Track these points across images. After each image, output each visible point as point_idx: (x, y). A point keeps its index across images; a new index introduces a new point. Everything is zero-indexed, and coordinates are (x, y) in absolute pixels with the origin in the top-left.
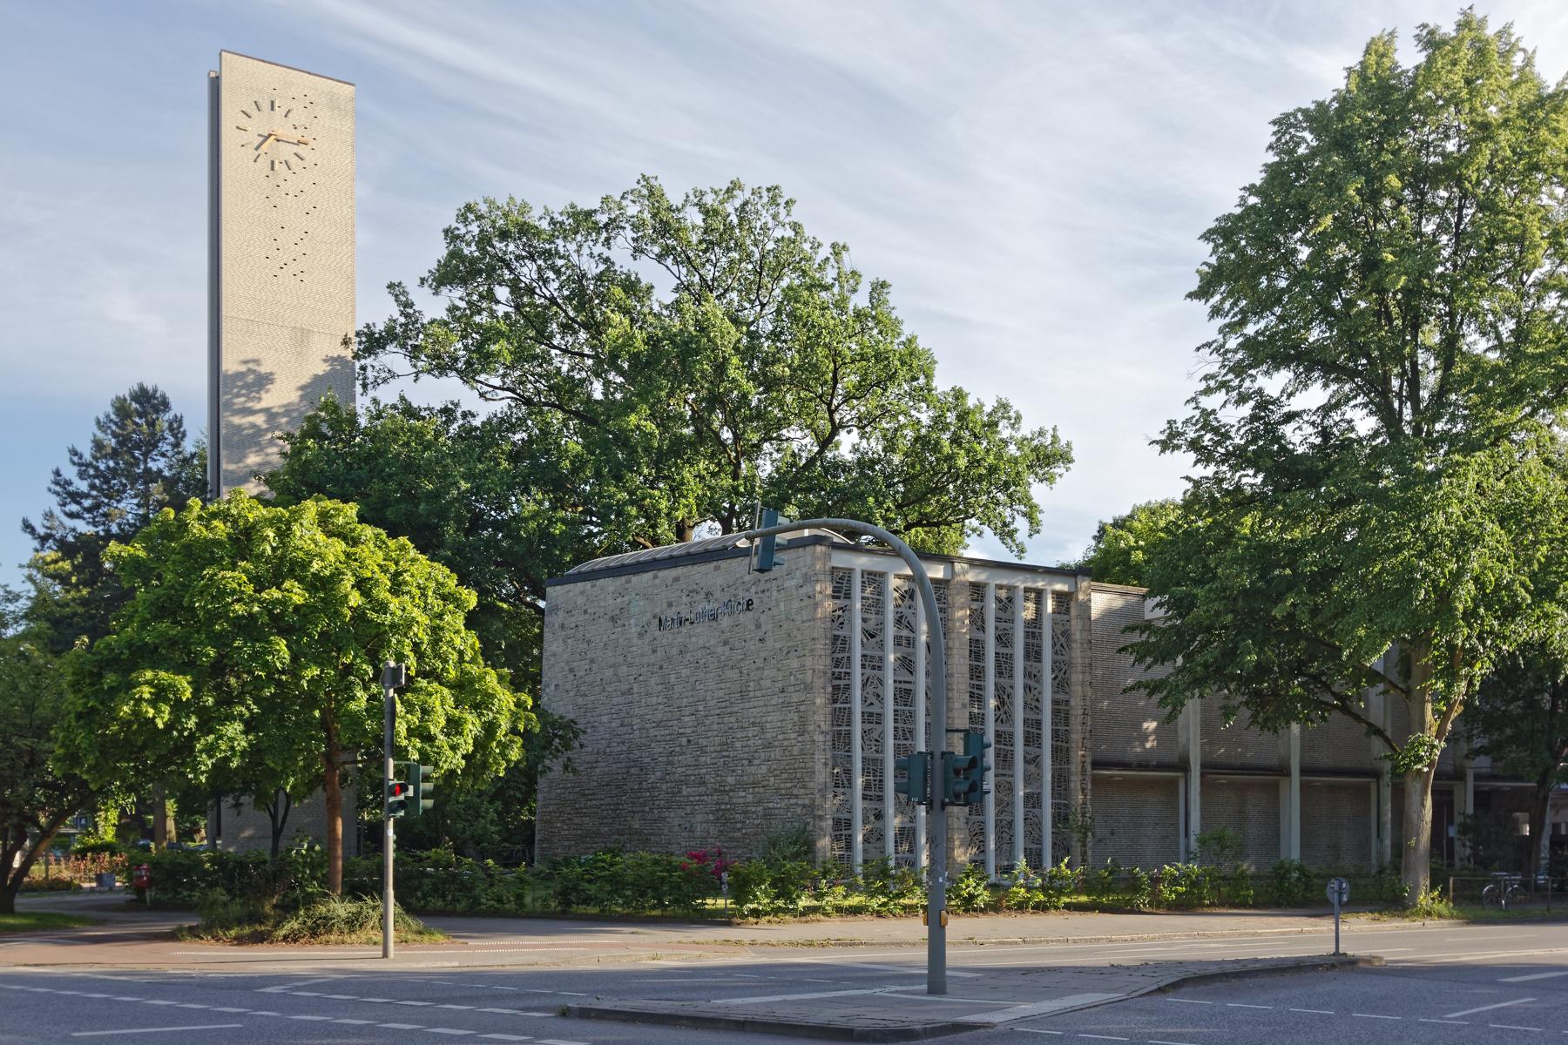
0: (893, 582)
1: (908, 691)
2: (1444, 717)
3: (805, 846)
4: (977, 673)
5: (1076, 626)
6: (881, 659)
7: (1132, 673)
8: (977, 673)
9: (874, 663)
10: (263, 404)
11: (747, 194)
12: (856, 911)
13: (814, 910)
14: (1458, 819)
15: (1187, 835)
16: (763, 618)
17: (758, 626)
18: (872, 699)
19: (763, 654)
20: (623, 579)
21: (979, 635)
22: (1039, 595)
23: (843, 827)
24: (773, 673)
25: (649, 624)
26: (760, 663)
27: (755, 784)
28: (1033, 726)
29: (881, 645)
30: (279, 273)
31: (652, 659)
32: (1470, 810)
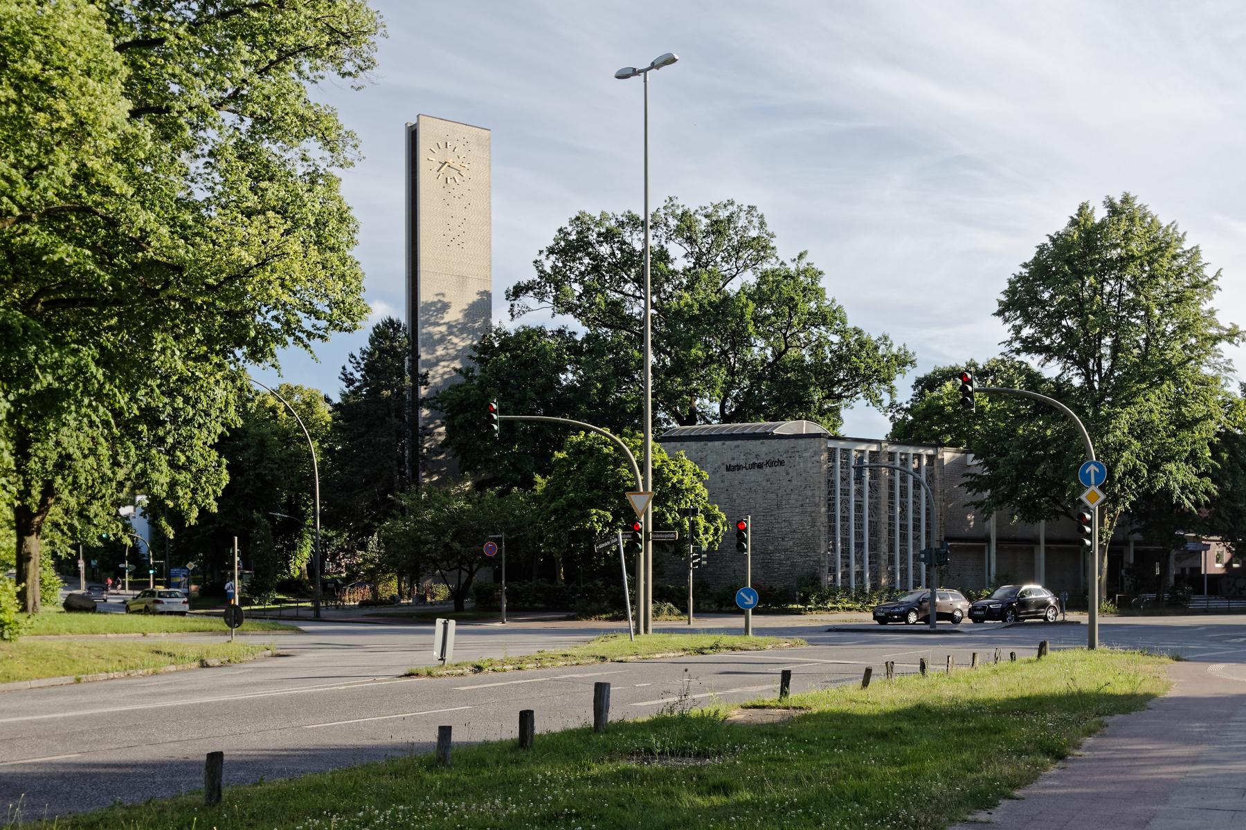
0: (854, 453)
1: (860, 506)
2: (1112, 520)
3: (814, 580)
4: (892, 496)
5: (937, 471)
6: (848, 490)
7: (968, 496)
8: (892, 496)
9: (845, 493)
10: (446, 320)
11: (735, 208)
12: (849, 609)
13: (832, 608)
14: (1126, 566)
15: (989, 574)
16: (790, 470)
17: (788, 474)
18: (844, 510)
19: (790, 487)
20: (702, 443)
21: (892, 477)
22: (919, 456)
23: (833, 570)
24: (796, 497)
25: (719, 467)
26: (788, 492)
27: (785, 550)
28: (917, 521)
29: (849, 484)
30: (450, 243)
31: (722, 485)
32: (1132, 561)
